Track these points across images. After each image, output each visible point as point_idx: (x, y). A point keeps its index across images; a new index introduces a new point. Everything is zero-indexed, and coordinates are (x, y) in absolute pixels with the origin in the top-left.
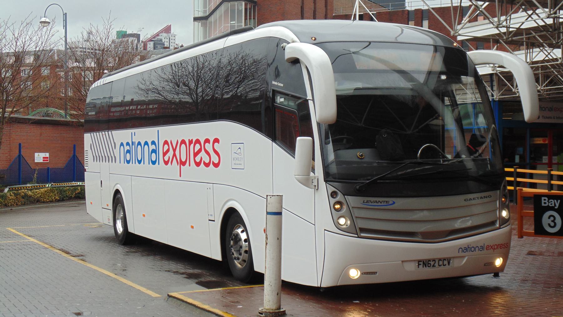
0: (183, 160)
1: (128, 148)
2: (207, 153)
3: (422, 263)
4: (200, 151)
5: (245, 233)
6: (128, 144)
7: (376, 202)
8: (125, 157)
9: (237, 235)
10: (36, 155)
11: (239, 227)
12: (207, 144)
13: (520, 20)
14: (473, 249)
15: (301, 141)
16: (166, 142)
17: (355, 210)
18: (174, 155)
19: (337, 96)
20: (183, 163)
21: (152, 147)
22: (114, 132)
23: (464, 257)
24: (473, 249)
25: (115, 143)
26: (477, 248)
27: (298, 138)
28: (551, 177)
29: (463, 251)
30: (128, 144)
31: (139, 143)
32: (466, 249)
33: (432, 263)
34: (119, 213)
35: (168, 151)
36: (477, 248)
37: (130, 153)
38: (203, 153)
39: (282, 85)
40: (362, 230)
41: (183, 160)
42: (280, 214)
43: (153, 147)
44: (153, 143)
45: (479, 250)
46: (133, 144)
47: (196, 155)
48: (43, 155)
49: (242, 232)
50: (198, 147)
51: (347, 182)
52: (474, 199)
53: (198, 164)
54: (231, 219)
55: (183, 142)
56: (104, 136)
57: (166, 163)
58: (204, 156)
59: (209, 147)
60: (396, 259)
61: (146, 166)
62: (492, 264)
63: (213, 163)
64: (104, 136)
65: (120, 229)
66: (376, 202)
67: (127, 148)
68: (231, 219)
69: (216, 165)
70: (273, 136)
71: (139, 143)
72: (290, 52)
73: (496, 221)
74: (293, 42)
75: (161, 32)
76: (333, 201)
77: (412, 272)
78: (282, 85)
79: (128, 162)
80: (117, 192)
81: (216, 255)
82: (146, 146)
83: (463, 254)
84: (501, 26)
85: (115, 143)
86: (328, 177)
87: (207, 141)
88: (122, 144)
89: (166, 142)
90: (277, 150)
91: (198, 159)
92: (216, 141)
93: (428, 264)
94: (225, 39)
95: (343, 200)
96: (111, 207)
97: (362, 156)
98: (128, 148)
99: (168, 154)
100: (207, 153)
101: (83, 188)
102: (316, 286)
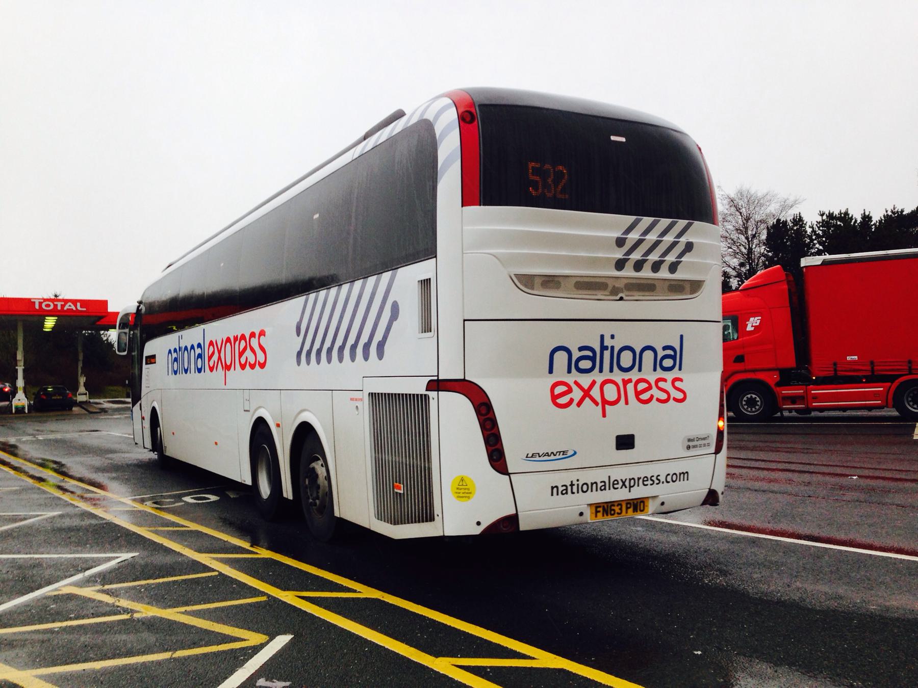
0: (228, 363)
3: (601, 509)
4: (245, 349)
7: (614, 484)
12: (252, 339)
14: (626, 359)
18: (220, 358)
20: (227, 368)
21: (198, 351)
24: (626, 359)
26: (648, 356)
29: (573, 365)
31: (186, 348)
33: (617, 509)
36: (648, 356)
38: (248, 353)
41: (228, 363)
45: (658, 364)
47: (241, 354)
53: (243, 367)
57: (211, 369)
67: (175, 355)
69: (262, 366)
71: (186, 348)
81: (249, 482)
89: (211, 343)
92: (262, 333)
93: (611, 510)
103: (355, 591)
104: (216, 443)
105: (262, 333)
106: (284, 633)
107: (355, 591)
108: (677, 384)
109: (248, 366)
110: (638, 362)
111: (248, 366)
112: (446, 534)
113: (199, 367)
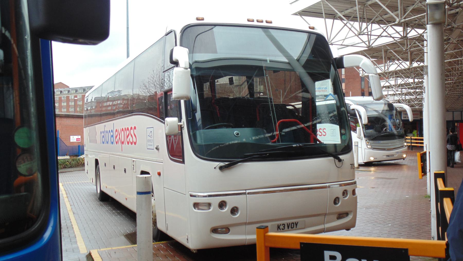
10: (71, 137)
13: (393, 67)
18: (119, 138)
19: (368, 118)
20: (123, 143)
21: (112, 134)
28: (411, 139)
32: (397, 152)
48: (76, 137)
60: (380, 155)
62: (402, 156)
67: (103, 134)
69: (324, 135)
84: (362, 33)
86: (365, 136)
89: (116, 131)
97: (238, 134)
104: (159, 174)
105: (135, 128)
106: (287, 59)
108: (324, 130)
109: (130, 143)
111: (130, 143)
112: (58, 121)
113: (59, 93)
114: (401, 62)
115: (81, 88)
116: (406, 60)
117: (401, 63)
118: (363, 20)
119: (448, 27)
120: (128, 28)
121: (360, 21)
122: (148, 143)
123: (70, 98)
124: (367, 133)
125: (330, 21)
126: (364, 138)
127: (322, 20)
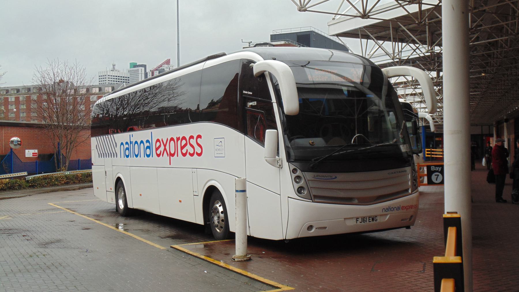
1: (127, 146)
2: (192, 146)
4: (186, 145)
5: (221, 207)
6: (127, 143)
7: (323, 176)
8: (125, 153)
9: (216, 208)
10: (27, 151)
11: (218, 203)
12: (191, 140)
15: (269, 133)
16: (158, 140)
17: (310, 182)
18: (165, 149)
20: (173, 155)
22: (116, 136)
23: (387, 215)
25: (116, 143)
27: (267, 131)
29: (385, 211)
30: (127, 143)
31: (136, 142)
34: (120, 190)
35: (160, 146)
37: (129, 151)
38: (188, 147)
39: (251, 93)
40: (316, 197)
42: (244, 191)
43: (148, 144)
44: (148, 141)
45: (397, 210)
46: (131, 143)
47: (182, 148)
48: (32, 151)
49: (220, 206)
50: (184, 142)
51: (305, 162)
52: (395, 173)
54: (212, 195)
55: (172, 139)
56: (107, 139)
57: (158, 155)
58: (190, 148)
59: (193, 142)
60: (337, 217)
61: (143, 160)
63: (197, 153)
64: (107, 139)
65: (122, 206)
66: (323, 176)
68: (212, 195)
69: (199, 155)
70: (244, 130)
71: (136, 142)
72: (256, 69)
73: (409, 189)
74: (259, 61)
75: (164, 64)
76: (294, 176)
77: (351, 226)
78: (251, 93)
79: (127, 156)
80: (119, 180)
81: (200, 221)
82: (142, 144)
83: (386, 213)
85: (116, 143)
86: (289, 159)
87: (192, 137)
88: (122, 144)
89: (158, 140)
90: (249, 142)
91: (184, 151)
92: (199, 136)
94: (204, 63)
95: (301, 175)
96: (113, 190)
97: (313, 143)
98: (127, 146)
99: (160, 149)
100: (192, 146)
101: (90, 175)
102: (282, 238)
103: (280, 288)
107: (280, 288)
110: (394, 210)
114: (417, 45)
115: (24, 88)
116: (424, 42)
117: (417, 48)
118: (395, 40)
119: (475, 11)
120: (178, 44)
121: (393, 41)
122: (216, 152)
123: (10, 100)
124: (298, 148)
125: (364, 41)
126: (286, 164)
127: (359, 40)
